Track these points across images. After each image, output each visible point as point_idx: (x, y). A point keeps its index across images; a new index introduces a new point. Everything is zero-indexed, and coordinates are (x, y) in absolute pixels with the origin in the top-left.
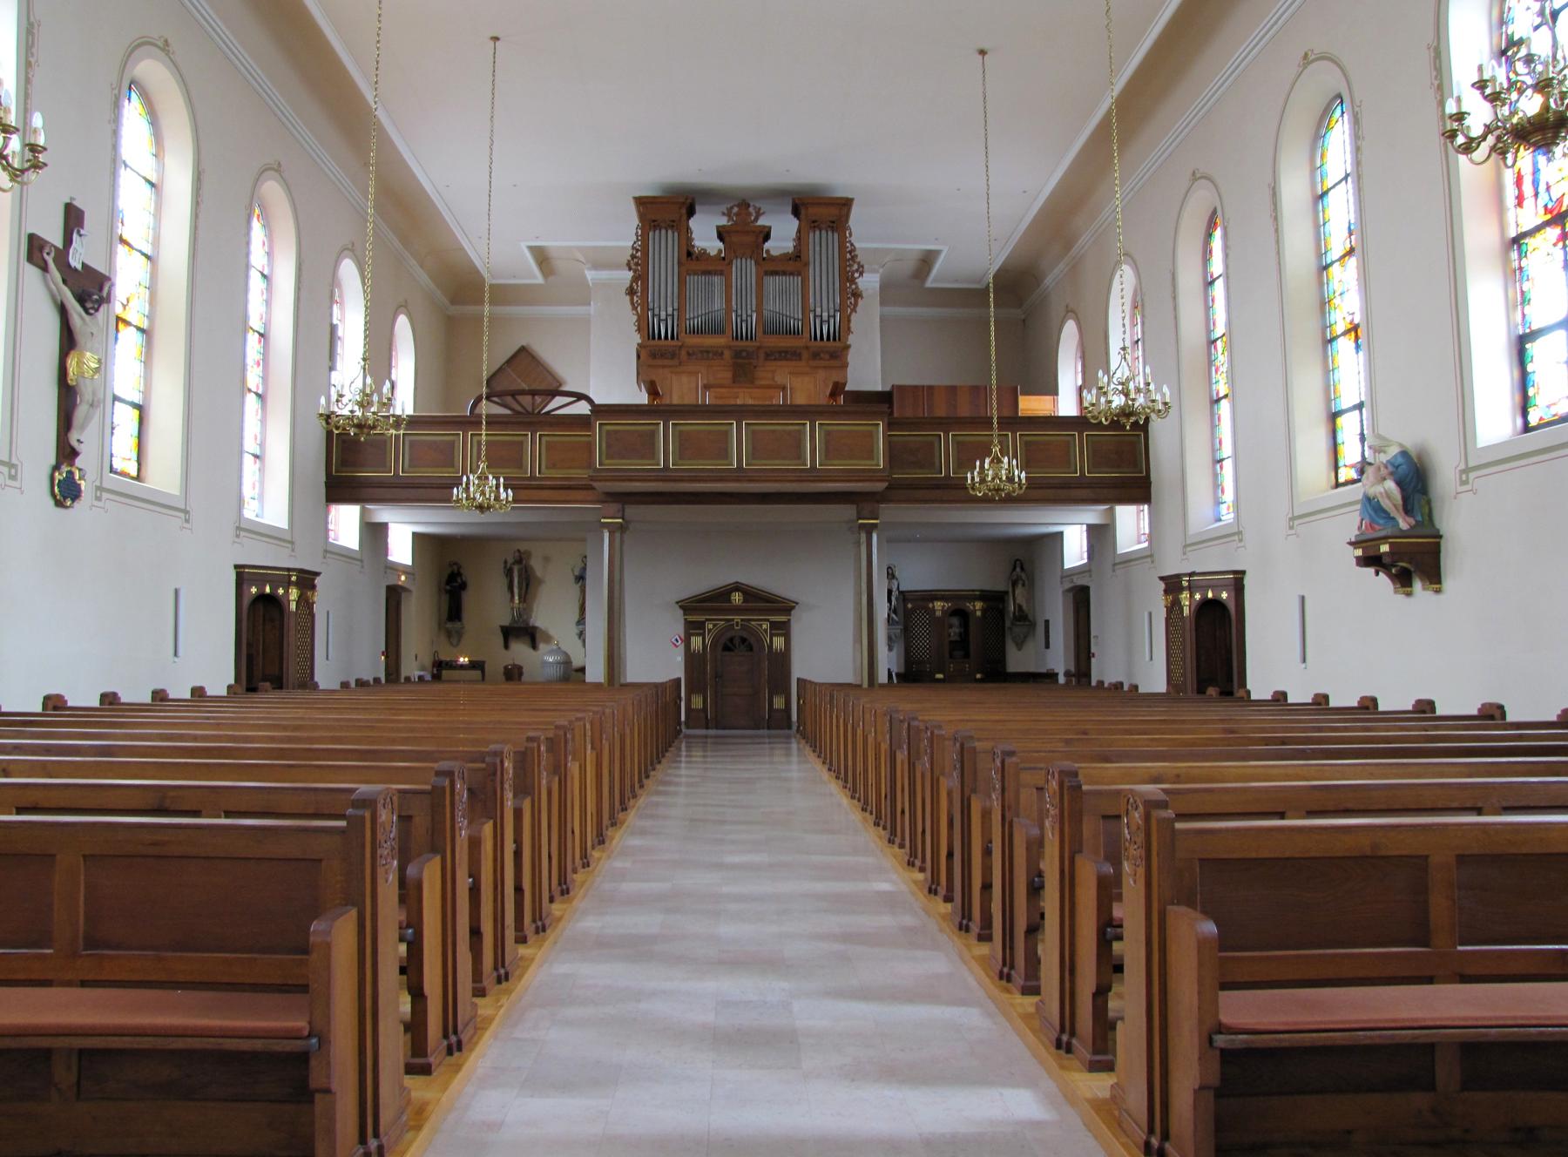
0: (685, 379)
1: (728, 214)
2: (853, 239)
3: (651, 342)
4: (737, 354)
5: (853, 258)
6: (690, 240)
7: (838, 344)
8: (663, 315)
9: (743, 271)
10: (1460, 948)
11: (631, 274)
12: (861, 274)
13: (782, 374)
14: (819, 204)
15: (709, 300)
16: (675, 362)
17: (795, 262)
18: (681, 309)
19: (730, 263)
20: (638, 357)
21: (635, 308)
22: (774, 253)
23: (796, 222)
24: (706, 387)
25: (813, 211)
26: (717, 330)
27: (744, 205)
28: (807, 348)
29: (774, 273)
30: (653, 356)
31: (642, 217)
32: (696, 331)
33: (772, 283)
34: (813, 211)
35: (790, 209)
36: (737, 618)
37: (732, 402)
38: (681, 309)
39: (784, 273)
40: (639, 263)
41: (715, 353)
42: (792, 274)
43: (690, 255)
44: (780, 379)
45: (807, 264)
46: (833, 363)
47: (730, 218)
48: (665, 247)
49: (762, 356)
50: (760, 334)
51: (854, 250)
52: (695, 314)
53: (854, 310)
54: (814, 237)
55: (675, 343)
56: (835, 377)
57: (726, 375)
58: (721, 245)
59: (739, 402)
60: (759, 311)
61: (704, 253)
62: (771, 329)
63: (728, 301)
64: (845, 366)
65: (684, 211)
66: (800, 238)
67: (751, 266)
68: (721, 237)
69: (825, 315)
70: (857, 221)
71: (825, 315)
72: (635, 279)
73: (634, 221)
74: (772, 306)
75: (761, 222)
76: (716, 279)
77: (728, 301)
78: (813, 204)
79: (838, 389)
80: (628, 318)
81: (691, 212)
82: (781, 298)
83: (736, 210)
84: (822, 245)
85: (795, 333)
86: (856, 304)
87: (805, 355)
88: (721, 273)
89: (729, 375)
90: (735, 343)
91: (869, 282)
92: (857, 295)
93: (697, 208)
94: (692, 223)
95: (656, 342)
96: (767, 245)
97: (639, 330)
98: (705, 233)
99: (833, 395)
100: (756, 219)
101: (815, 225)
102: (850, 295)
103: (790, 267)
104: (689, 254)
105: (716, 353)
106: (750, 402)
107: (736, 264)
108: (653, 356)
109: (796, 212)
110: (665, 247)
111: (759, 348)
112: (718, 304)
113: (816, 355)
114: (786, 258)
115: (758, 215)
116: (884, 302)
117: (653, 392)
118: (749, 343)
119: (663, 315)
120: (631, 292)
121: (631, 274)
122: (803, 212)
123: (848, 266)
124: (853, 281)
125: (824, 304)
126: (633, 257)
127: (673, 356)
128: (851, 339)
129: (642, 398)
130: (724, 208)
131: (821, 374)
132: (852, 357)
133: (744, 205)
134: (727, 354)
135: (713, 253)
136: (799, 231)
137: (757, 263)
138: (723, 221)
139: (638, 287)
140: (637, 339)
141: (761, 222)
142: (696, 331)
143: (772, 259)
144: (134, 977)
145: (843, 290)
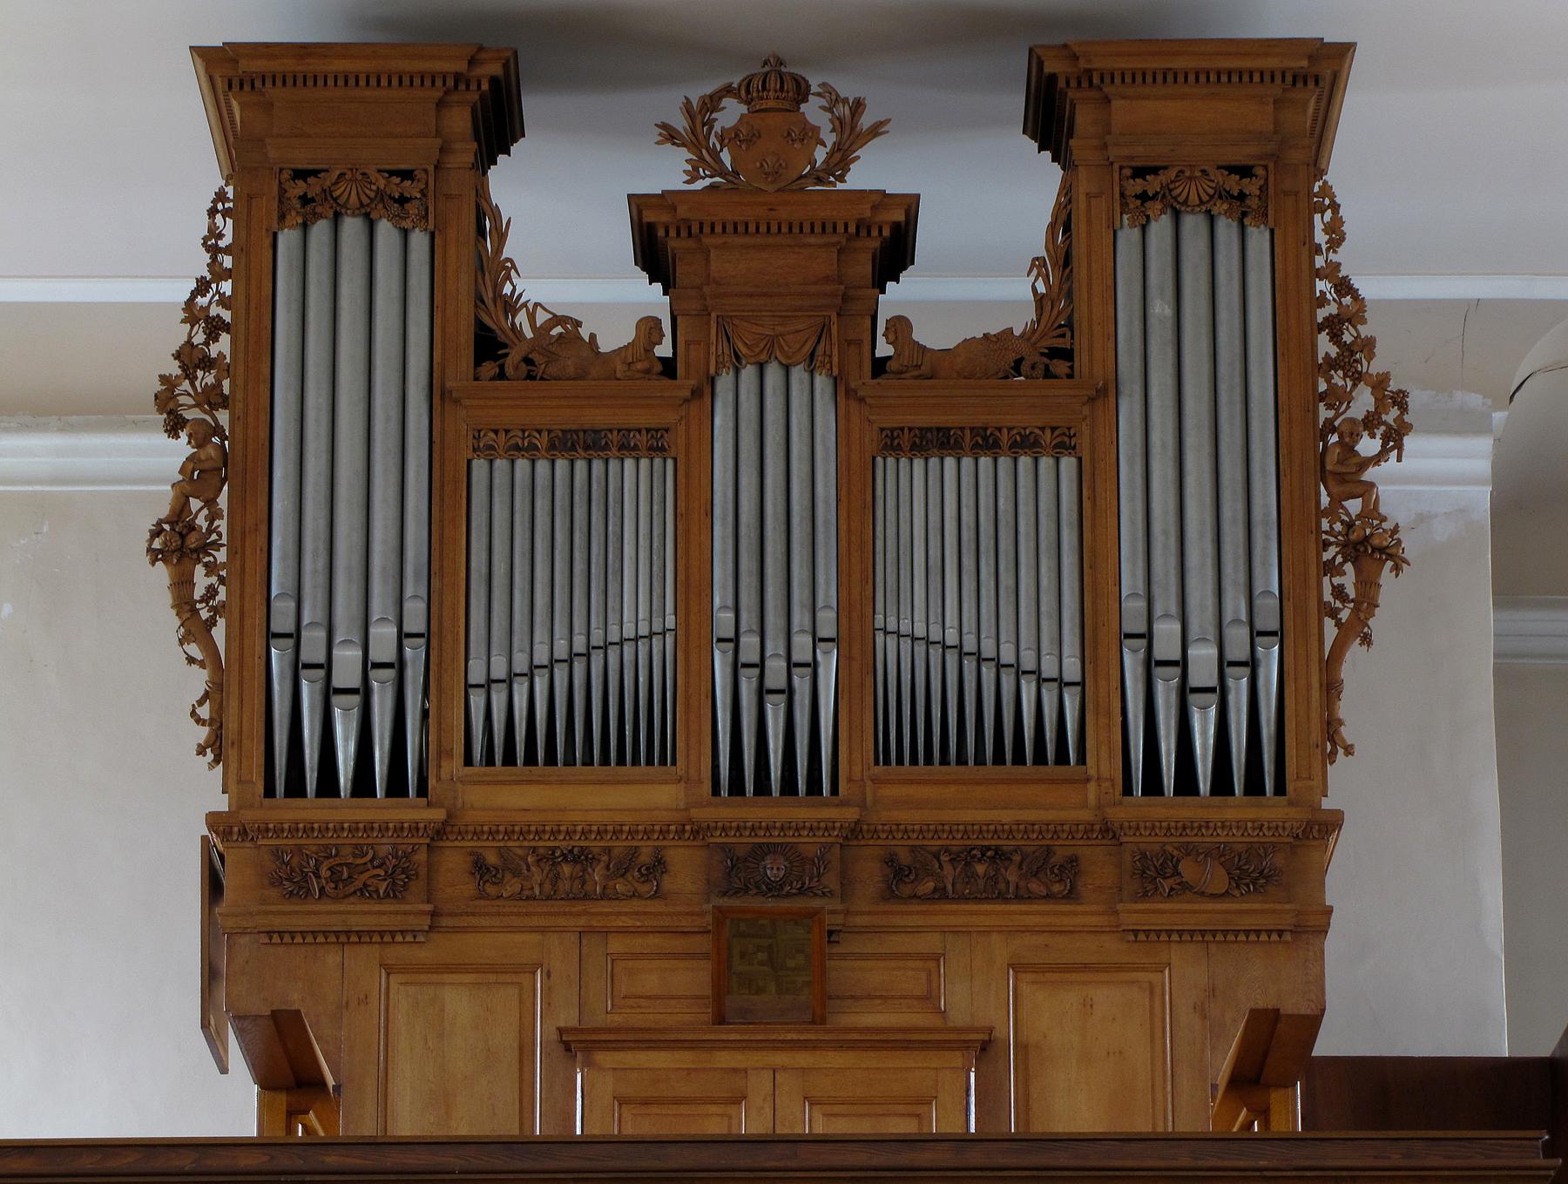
0: (458, 1001)
1: (693, 133)
2: (1348, 259)
3: (289, 811)
4: (739, 868)
5: (1351, 358)
6: (491, 269)
7: (1271, 809)
8: (347, 671)
9: (778, 428)
10: (579, 1077)
11: (181, 448)
12: (1394, 439)
13: (974, 971)
14: (1169, 76)
15: (586, 585)
16: (413, 910)
17: (1042, 388)
18: (441, 636)
19: (705, 390)
20: (213, 886)
21: (194, 628)
22: (934, 335)
23: (1056, 172)
24: (575, 1045)
25: (1144, 118)
26: (625, 736)
27: (776, 86)
28: (1109, 831)
29: (936, 441)
30: (295, 876)
31: (240, 151)
32: (524, 751)
33: (923, 493)
34: (1144, 118)
35: (1015, 103)
36: (771, 104)
37: (714, 1127)
38: (441, 636)
39: (986, 442)
40: (222, 391)
41: (624, 866)
42: (1025, 444)
43: (491, 353)
44: (974, 990)
45: (1105, 392)
46: (1249, 910)
47: (703, 160)
48: (363, 304)
49: (869, 871)
50: (858, 760)
51: (1355, 313)
52: (518, 652)
53: (1357, 630)
54: (1142, 254)
55: (410, 811)
56: (1259, 982)
57: (674, 982)
58: (651, 297)
59: (747, 1123)
60: (856, 635)
61: (564, 335)
62: (921, 737)
63: (692, 588)
64: (1310, 926)
65: (460, 120)
66: (1066, 256)
67: (808, 410)
68: (653, 256)
69: (1203, 657)
70: (1368, 161)
71: (1203, 657)
72: (198, 479)
73: (200, 172)
74: (925, 614)
75: (860, 177)
76: (632, 476)
77: (692, 588)
78: (1139, 77)
79: (1274, 1049)
80: (166, 683)
81: (498, 129)
82: (973, 581)
83: (731, 113)
84: (1186, 293)
85: (1050, 752)
86: (1366, 602)
87: (1100, 868)
88: (655, 444)
89: (693, 979)
90: (729, 811)
91: (1436, 479)
92: (1372, 549)
93: (533, 106)
94: (510, 184)
95: (311, 809)
96: (897, 296)
97: (216, 746)
98: (569, 232)
99: (1250, 1080)
100: (841, 160)
101: (1145, 187)
102: (1340, 551)
103: (1022, 405)
104: (488, 345)
105: (632, 863)
106: (811, 1122)
107: (734, 395)
108: (295, 876)
109: (1048, 124)
110: (363, 304)
111: (855, 831)
112: (638, 606)
113: (1156, 873)
114: (997, 359)
115: (853, 134)
116: (1512, 587)
117: (288, 1073)
118: (802, 811)
119: (347, 671)
120: (177, 543)
121: (181, 448)
122: (1085, 119)
123: (1327, 395)
124: (1349, 476)
125: (1197, 595)
126: (191, 359)
127: (399, 877)
128: (1343, 786)
129: (228, 1106)
130: (669, 105)
131: (1185, 973)
132: (1347, 878)
133: (776, 86)
134: (686, 871)
135: (614, 336)
136: (1063, 221)
137: (843, 389)
138: (668, 172)
139: (216, 519)
140: (207, 791)
141: (860, 177)
142: (524, 751)
143: (921, 366)
144: (1288, 713)
145: (1295, 522)
